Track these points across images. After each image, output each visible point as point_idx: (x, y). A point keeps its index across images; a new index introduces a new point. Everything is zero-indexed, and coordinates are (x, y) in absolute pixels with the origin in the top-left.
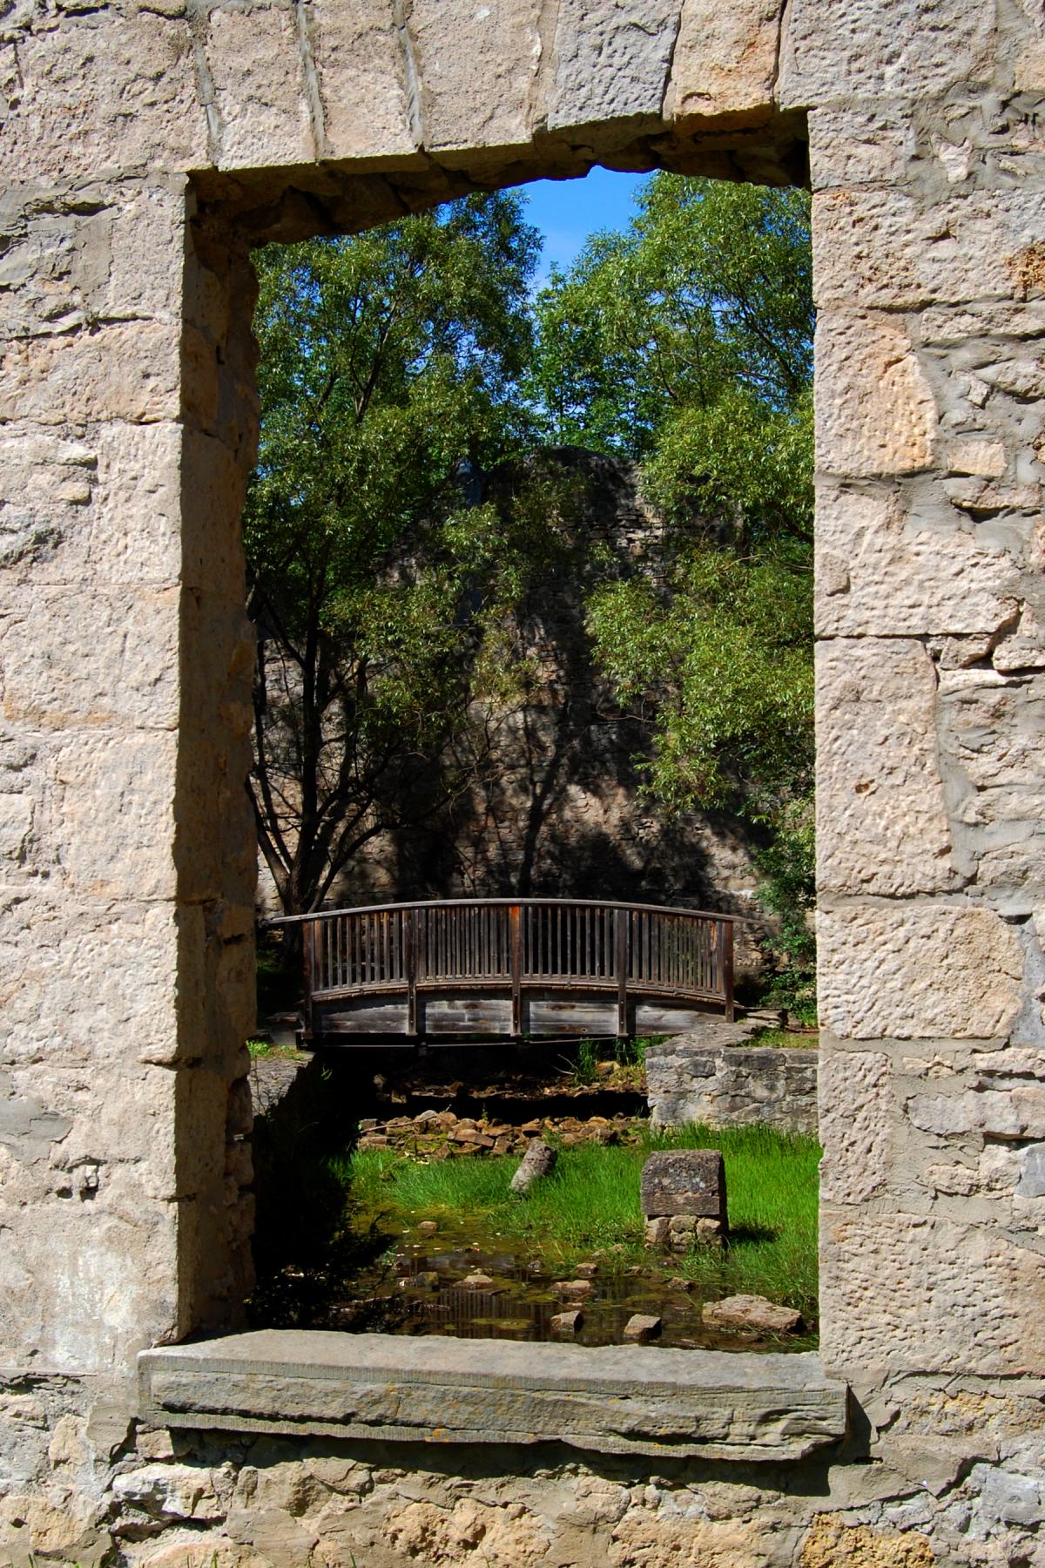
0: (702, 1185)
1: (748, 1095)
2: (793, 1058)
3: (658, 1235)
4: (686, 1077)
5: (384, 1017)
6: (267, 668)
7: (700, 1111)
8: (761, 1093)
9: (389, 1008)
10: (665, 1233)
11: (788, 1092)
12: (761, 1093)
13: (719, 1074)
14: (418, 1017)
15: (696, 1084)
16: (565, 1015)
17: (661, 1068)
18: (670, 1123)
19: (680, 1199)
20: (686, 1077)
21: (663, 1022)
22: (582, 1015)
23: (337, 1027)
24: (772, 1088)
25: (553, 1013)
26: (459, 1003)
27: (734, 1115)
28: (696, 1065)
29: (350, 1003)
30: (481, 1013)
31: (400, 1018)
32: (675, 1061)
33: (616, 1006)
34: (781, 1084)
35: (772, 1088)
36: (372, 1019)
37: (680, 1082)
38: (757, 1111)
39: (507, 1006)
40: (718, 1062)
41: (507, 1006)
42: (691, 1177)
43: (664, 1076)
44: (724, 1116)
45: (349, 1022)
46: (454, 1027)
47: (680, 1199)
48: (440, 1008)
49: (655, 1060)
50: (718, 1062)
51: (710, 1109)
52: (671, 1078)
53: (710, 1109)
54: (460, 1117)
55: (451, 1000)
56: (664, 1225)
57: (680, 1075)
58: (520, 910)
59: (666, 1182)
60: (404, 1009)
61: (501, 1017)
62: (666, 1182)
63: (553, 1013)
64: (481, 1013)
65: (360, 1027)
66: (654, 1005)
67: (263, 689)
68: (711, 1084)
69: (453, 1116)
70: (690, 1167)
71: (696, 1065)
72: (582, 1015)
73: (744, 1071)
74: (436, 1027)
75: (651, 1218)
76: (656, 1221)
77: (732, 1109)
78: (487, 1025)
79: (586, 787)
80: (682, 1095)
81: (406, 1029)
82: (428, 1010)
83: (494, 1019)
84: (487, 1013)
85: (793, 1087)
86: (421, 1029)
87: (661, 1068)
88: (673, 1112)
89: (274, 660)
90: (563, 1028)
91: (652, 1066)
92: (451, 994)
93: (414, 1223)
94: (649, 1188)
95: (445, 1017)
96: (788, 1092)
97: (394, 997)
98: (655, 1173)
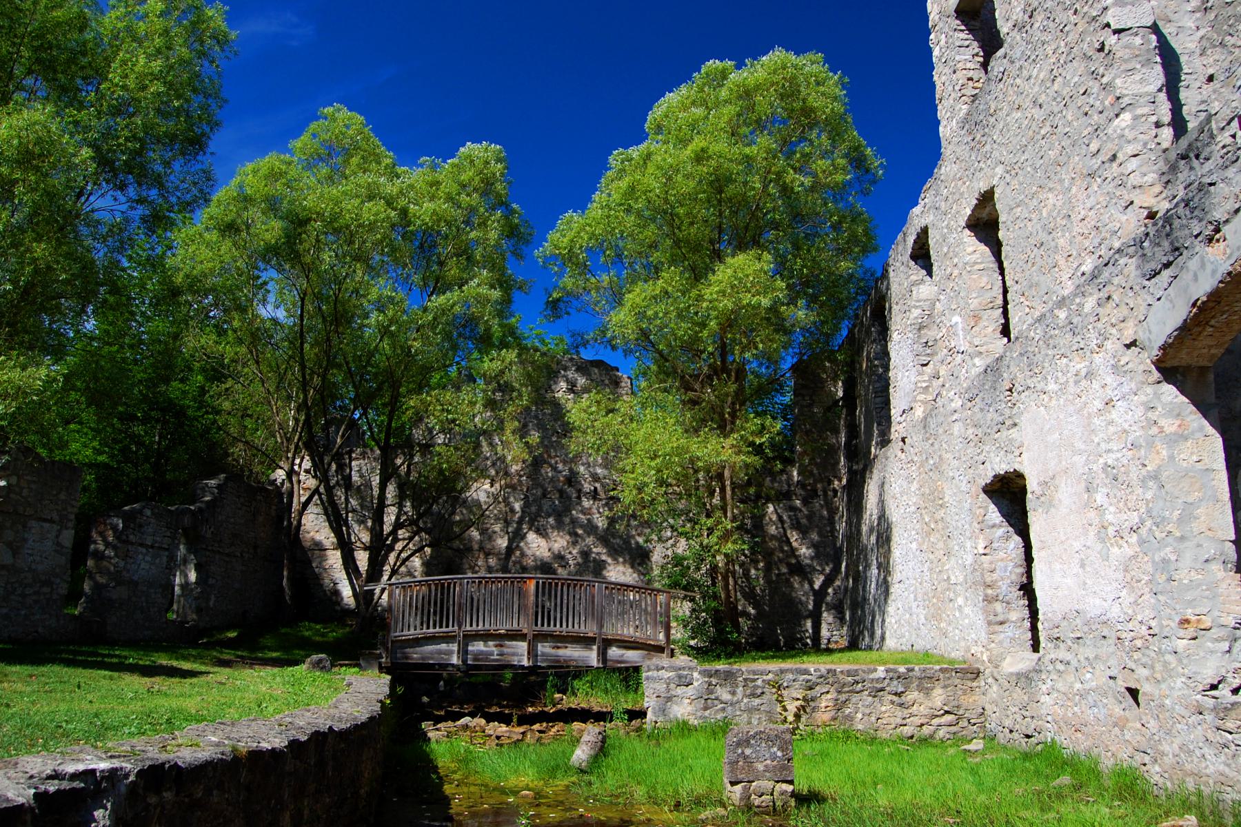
0: (779, 754)
1: (717, 699)
2: (749, 672)
3: (741, 799)
4: (672, 686)
5: (440, 652)
6: (353, 463)
7: (683, 709)
8: (726, 696)
9: (443, 646)
10: (746, 797)
11: (745, 696)
12: (726, 696)
13: (696, 684)
14: (464, 652)
15: (680, 691)
16: (561, 652)
17: (654, 679)
18: (661, 719)
19: (760, 767)
20: (672, 686)
21: (625, 658)
22: (572, 653)
23: (407, 658)
24: (733, 693)
25: (553, 651)
26: (491, 643)
27: (707, 713)
28: (680, 677)
29: (418, 642)
30: (505, 650)
31: (450, 653)
32: (665, 674)
33: (595, 647)
34: (740, 690)
35: (733, 693)
36: (432, 653)
37: (668, 690)
38: (723, 709)
39: (523, 646)
40: (696, 675)
41: (523, 646)
42: (770, 747)
43: (657, 686)
44: (699, 714)
45: (416, 654)
46: (487, 660)
47: (760, 767)
48: (478, 646)
49: (650, 673)
50: (696, 675)
51: (689, 708)
52: (662, 687)
53: (689, 708)
54: (488, 722)
55: (485, 641)
56: (746, 789)
57: (668, 684)
58: (534, 582)
59: (748, 752)
60: (454, 647)
61: (519, 653)
62: (748, 752)
63: (553, 651)
64: (505, 650)
65: (423, 658)
66: (619, 647)
67: (350, 476)
68: (690, 691)
69: (483, 721)
70: (768, 739)
71: (680, 677)
72: (572, 653)
73: (714, 681)
74: (475, 659)
75: (733, 784)
76: (738, 788)
77: (706, 709)
78: (509, 658)
79: (538, 532)
80: (669, 699)
81: (455, 660)
82: (470, 648)
83: (513, 654)
84: (509, 650)
85: (748, 692)
86: (465, 661)
87: (654, 679)
88: (663, 711)
89: (357, 459)
90: (558, 661)
91: (647, 678)
92: (486, 636)
93: (515, 793)
94: (733, 757)
95: (481, 652)
96: (745, 696)
97: (448, 638)
98: (739, 744)
